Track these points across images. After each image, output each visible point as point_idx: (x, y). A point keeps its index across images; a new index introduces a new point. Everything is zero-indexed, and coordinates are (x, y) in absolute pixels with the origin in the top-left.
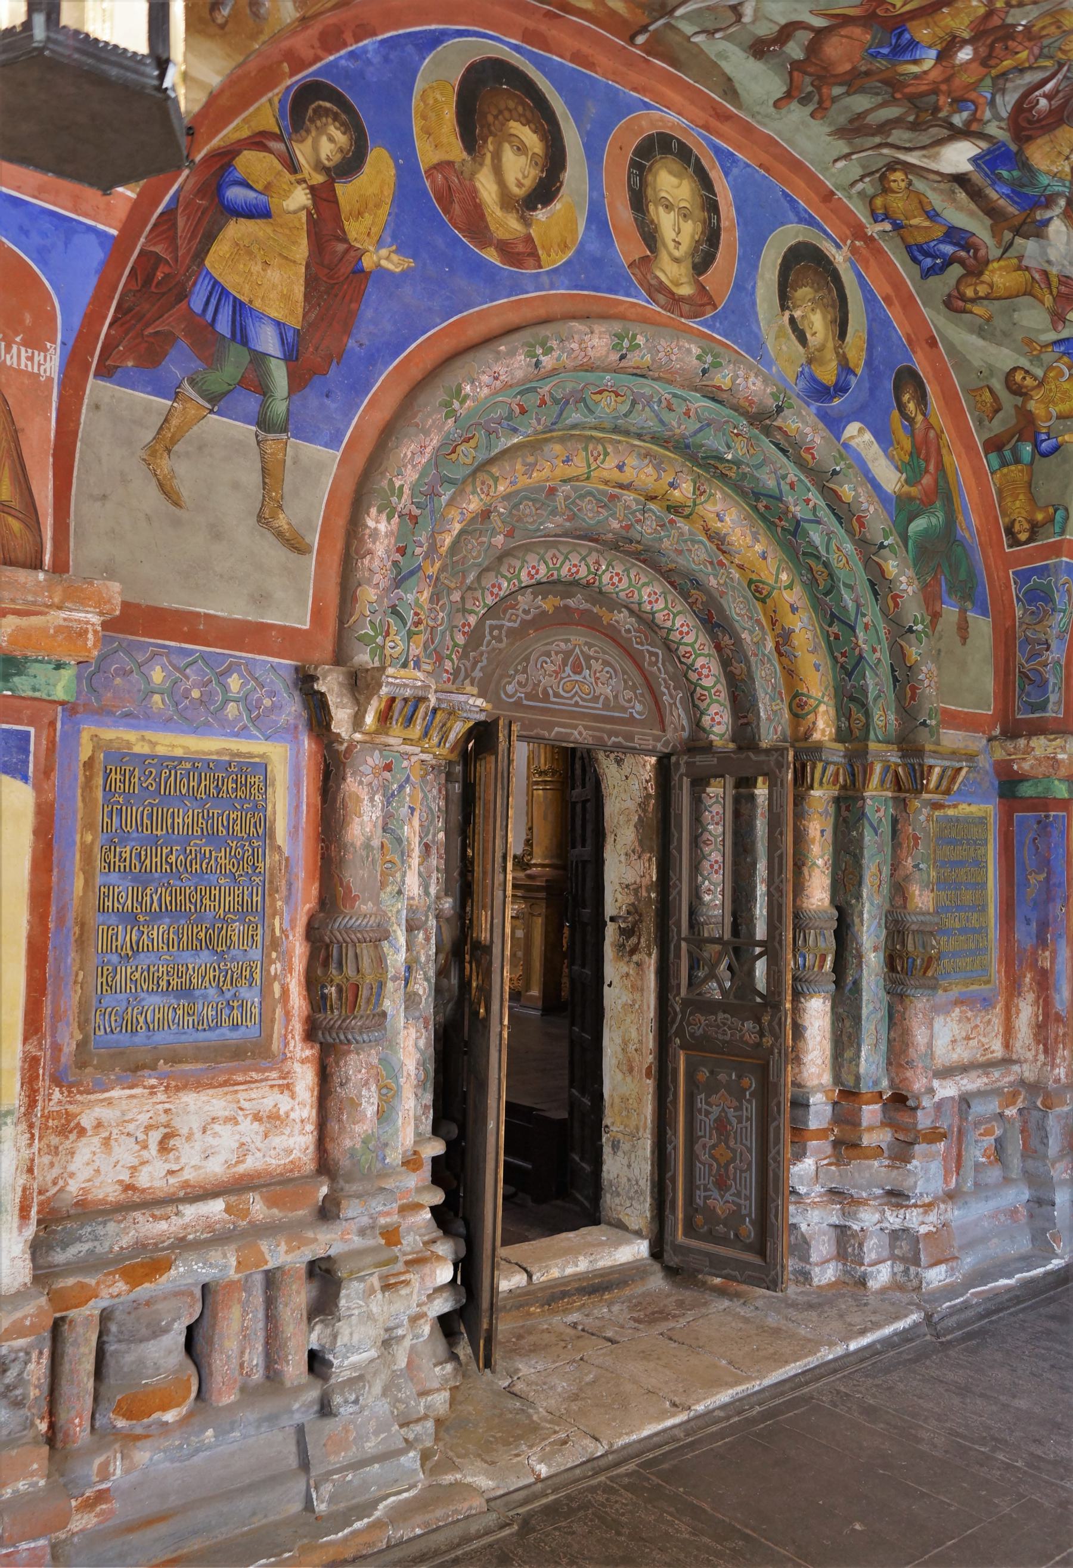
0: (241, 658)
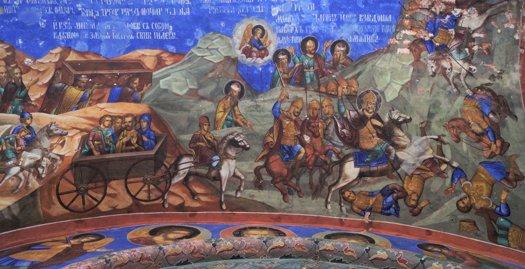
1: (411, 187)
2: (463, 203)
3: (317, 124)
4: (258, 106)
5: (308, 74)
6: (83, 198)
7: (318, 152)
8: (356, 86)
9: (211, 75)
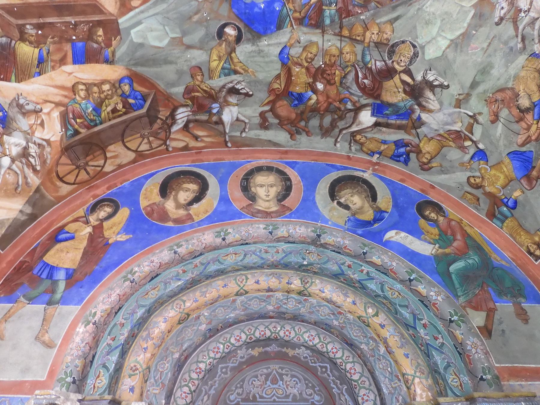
0: (7, 397)
1: (428, 148)
2: (475, 180)
3: (333, 72)
4: (260, 51)
5: (327, 13)
6: (85, 170)
7: (332, 99)
8: (389, 33)
9: (196, 18)
